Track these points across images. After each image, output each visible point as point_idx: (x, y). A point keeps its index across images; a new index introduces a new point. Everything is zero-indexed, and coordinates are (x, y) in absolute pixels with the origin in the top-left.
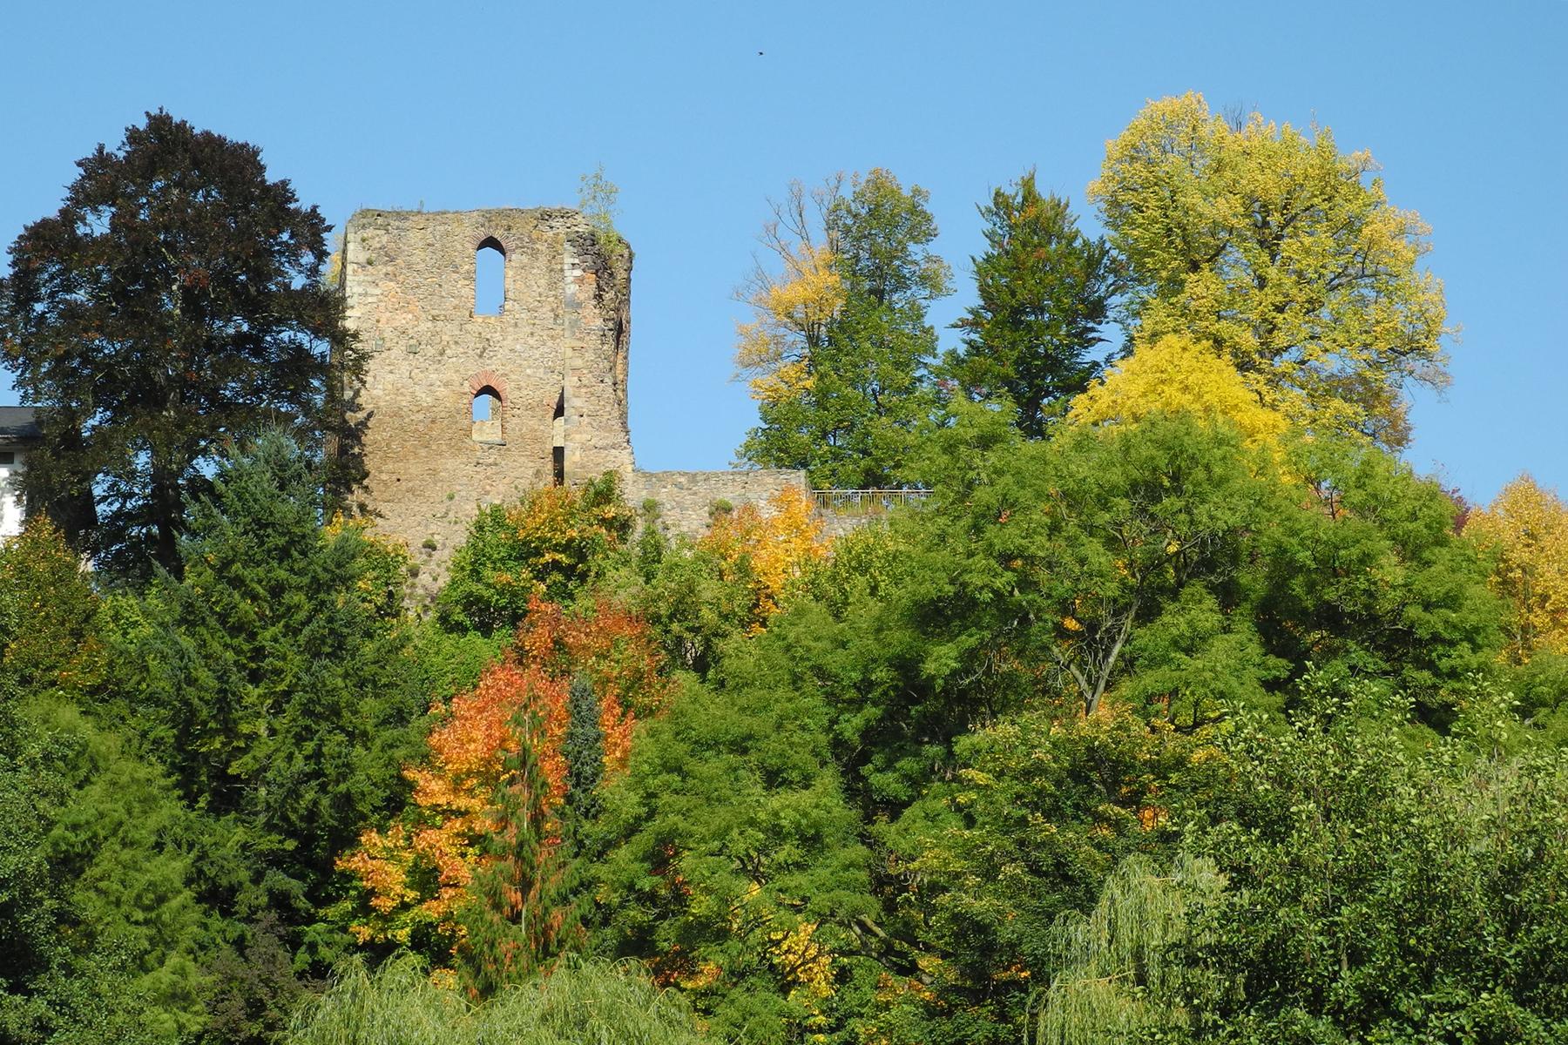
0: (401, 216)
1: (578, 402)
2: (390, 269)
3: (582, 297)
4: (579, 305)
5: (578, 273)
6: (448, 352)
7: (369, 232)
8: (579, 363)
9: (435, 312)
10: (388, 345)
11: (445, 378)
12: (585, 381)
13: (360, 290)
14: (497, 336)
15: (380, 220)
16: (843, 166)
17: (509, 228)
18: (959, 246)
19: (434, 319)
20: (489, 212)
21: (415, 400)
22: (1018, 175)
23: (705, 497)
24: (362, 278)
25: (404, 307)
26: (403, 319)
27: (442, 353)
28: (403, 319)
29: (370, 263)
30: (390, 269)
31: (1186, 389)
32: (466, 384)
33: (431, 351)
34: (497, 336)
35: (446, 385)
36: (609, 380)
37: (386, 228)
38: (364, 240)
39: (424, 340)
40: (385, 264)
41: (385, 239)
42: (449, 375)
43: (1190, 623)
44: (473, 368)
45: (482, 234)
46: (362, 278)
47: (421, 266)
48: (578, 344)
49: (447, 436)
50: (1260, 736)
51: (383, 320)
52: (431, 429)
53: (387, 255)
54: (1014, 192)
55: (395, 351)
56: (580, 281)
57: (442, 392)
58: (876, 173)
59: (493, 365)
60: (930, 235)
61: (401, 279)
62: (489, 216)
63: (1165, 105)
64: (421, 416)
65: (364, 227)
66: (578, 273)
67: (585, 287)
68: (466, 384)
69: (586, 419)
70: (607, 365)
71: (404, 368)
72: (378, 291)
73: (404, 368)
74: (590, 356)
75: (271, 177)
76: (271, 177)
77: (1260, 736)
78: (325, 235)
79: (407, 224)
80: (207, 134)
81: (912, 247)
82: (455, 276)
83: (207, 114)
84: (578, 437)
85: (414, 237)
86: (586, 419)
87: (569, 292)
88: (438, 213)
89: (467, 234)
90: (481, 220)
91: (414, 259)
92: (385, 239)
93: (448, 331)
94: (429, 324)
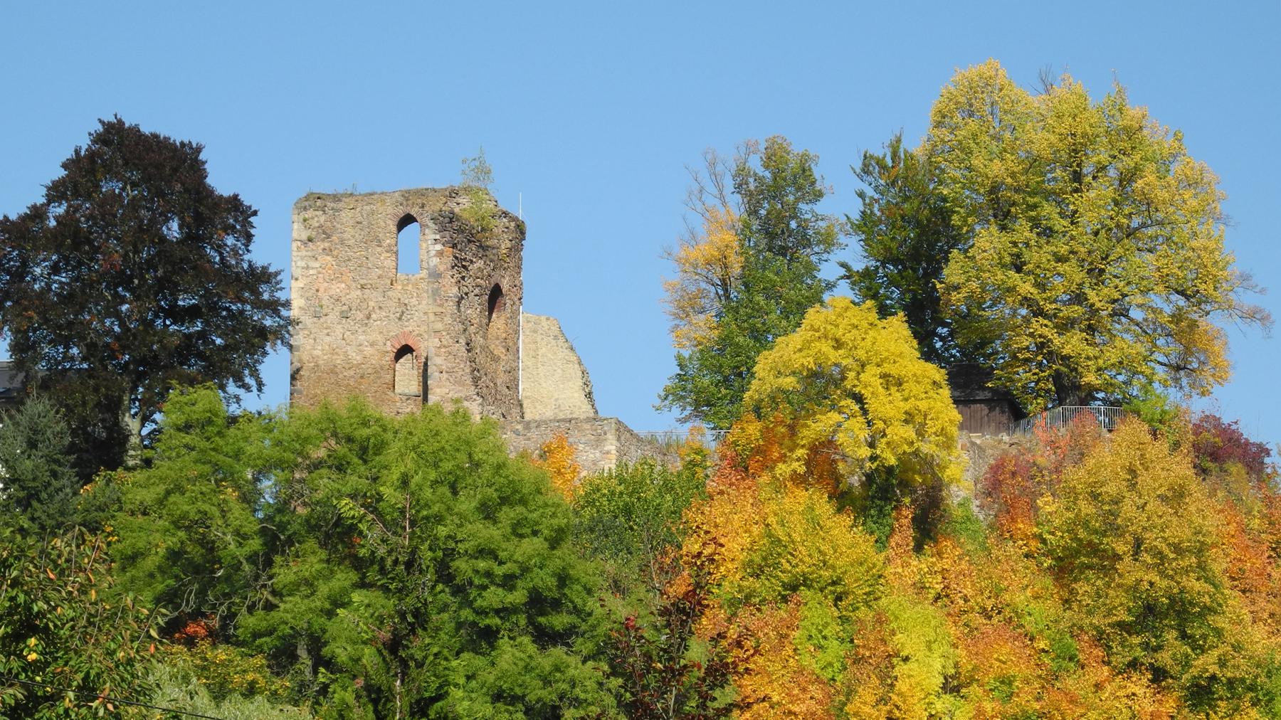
0: (336, 198)
1: (438, 361)
2: (327, 245)
4: (439, 275)
5: (439, 247)
6: (374, 316)
8: (439, 326)
9: (362, 282)
10: (325, 311)
11: (371, 338)
12: (445, 343)
13: (303, 264)
15: (319, 203)
16: (739, 138)
17: (423, 206)
19: (362, 287)
20: (408, 192)
21: (347, 359)
22: (889, 138)
23: (536, 442)
24: (304, 253)
25: (338, 277)
26: (338, 288)
27: (368, 318)
28: (338, 288)
29: (310, 240)
30: (327, 245)
31: (838, 344)
32: (389, 343)
33: (360, 316)
35: (372, 345)
37: (323, 209)
38: (305, 220)
39: (354, 306)
40: (323, 240)
41: (322, 219)
42: (375, 336)
44: (394, 330)
45: (401, 212)
46: (304, 253)
47: (351, 242)
48: (439, 310)
49: (373, 389)
50: (113, 646)
51: (322, 290)
52: (360, 384)
53: (324, 233)
54: (880, 150)
55: (330, 316)
56: (440, 254)
57: (369, 351)
59: (410, 326)
60: (819, 195)
61: (335, 253)
62: (407, 195)
63: (973, 72)
64: (352, 373)
65: (305, 209)
66: (439, 247)
67: (445, 260)
68: (389, 343)
69: (445, 375)
70: (461, 327)
72: (317, 265)
73: (339, 330)
74: (448, 320)
77: (113, 646)
79: (340, 205)
81: (803, 206)
82: (379, 249)
83: (151, 120)
84: (438, 390)
85: (346, 216)
86: (445, 375)
87: (432, 264)
88: (366, 195)
89: (388, 215)
91: (345, 236)
92: (322, 219)
93: (374, 298)
94: (359, 293)
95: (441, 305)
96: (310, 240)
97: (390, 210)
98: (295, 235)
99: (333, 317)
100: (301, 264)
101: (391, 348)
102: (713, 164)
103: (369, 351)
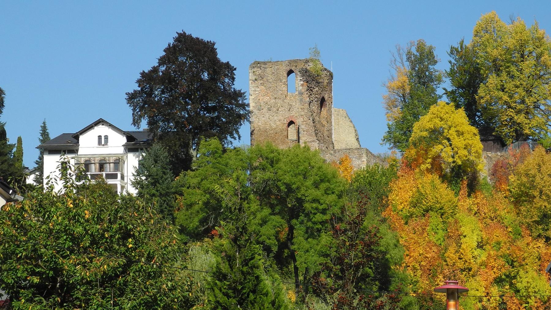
0: (265, 63)
3: (303, 91)
7: (255, 69)
8: (303, 113)
9: (275, 96)
10: (262, 108)
14: (294, 104)
16: (408, 40)
18: (443, 64)
20: (291, 61)
21: (271, 127)
22: (459, 40)
26: (266, 99)
28: (266, 99)
29: (256, 80)
31: (442, 119)
33: (275, 109)
34: (294, 104)
36: (311, 119)
37: (260, 67)
43: (63, 263)
45: (288, 69)
47: (270, 81)
49: (280, 138)
54: (457, 45)
57: (278, 123)
58: (420, 41)
60: (436, 62)
62: (290, 62)
65: (254, 67)
66: (302, 82)
71: (267, 115)
72: (259, 90)
73: (267, 115)
75: (164, 53)
76: (164, 53)
78: (234, 72)
79: (266, 66)
80: (198, 39)
85: (268, 70)
88: (275, 62)
89: (284, 70)
90: (288, 64)
91: (268, 78)
92: (260, 72)
94: (274, 100)
95: (303, 105)
96: (256, 80)
97: (284, 68)
98: (250, 78)
99: (265, 110)
100: (253, 89)
101: (286, 122)
102: (399, 50)
103: (278, 123)
